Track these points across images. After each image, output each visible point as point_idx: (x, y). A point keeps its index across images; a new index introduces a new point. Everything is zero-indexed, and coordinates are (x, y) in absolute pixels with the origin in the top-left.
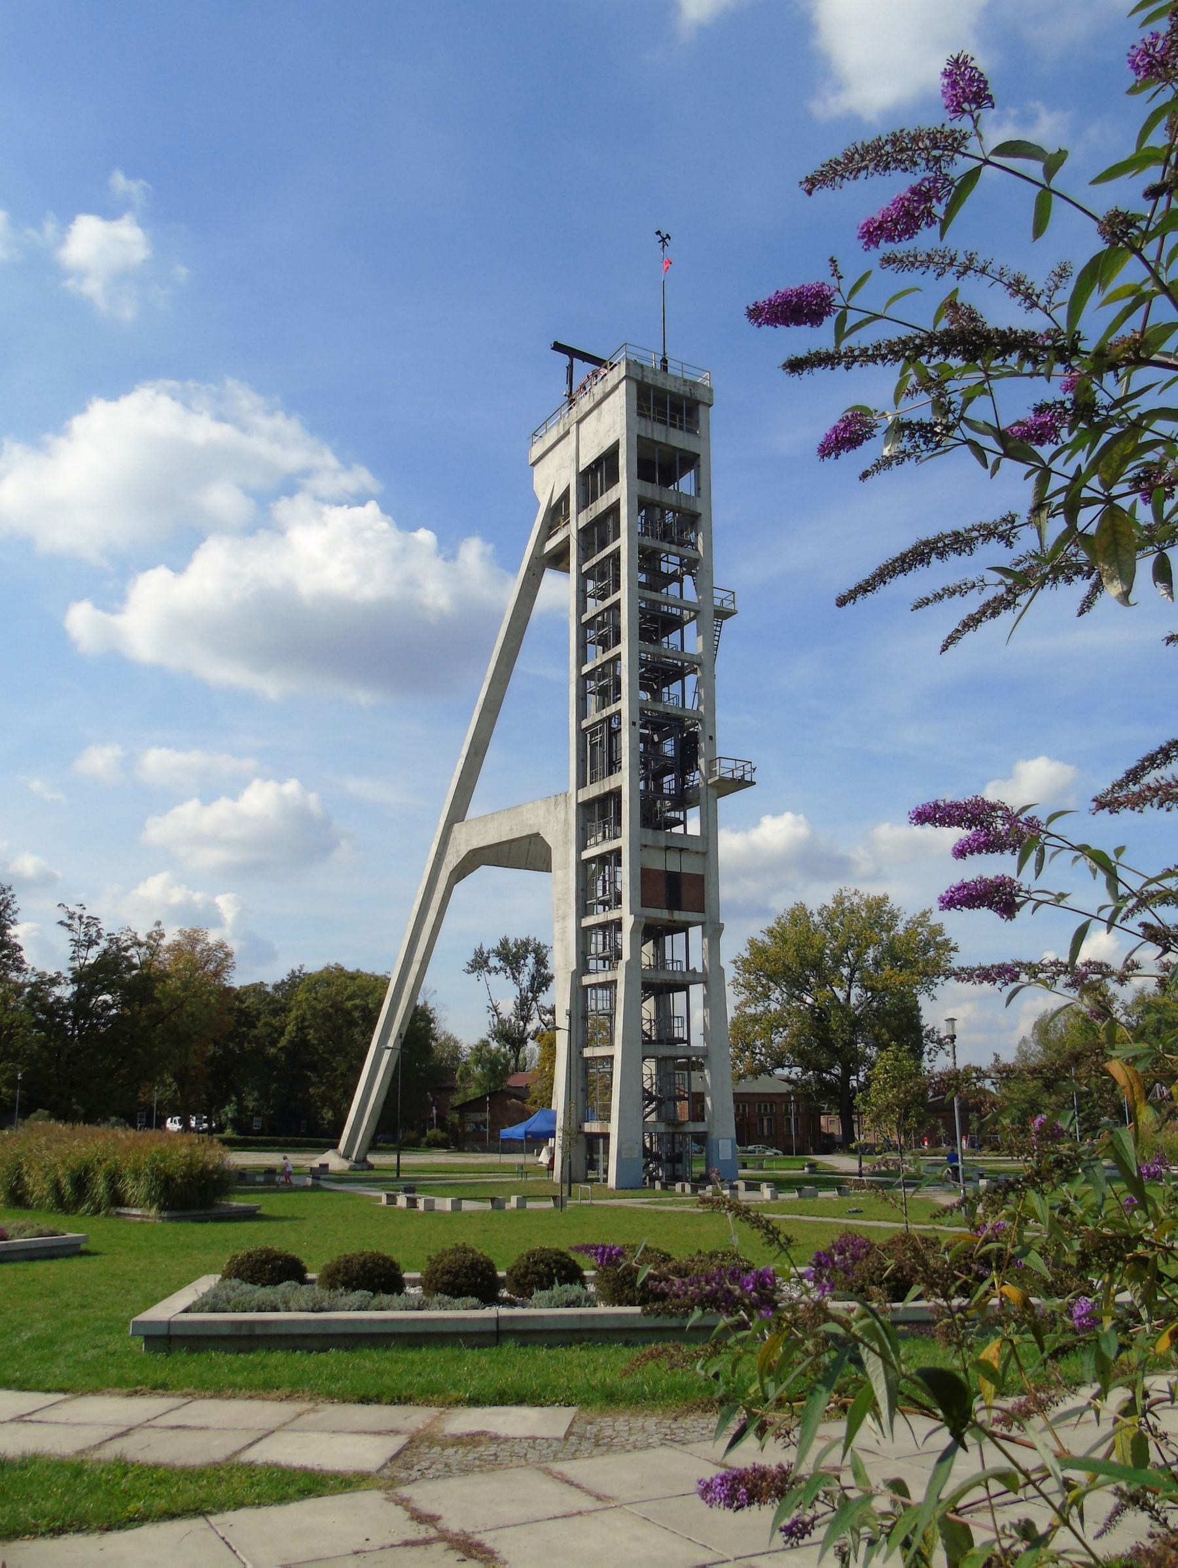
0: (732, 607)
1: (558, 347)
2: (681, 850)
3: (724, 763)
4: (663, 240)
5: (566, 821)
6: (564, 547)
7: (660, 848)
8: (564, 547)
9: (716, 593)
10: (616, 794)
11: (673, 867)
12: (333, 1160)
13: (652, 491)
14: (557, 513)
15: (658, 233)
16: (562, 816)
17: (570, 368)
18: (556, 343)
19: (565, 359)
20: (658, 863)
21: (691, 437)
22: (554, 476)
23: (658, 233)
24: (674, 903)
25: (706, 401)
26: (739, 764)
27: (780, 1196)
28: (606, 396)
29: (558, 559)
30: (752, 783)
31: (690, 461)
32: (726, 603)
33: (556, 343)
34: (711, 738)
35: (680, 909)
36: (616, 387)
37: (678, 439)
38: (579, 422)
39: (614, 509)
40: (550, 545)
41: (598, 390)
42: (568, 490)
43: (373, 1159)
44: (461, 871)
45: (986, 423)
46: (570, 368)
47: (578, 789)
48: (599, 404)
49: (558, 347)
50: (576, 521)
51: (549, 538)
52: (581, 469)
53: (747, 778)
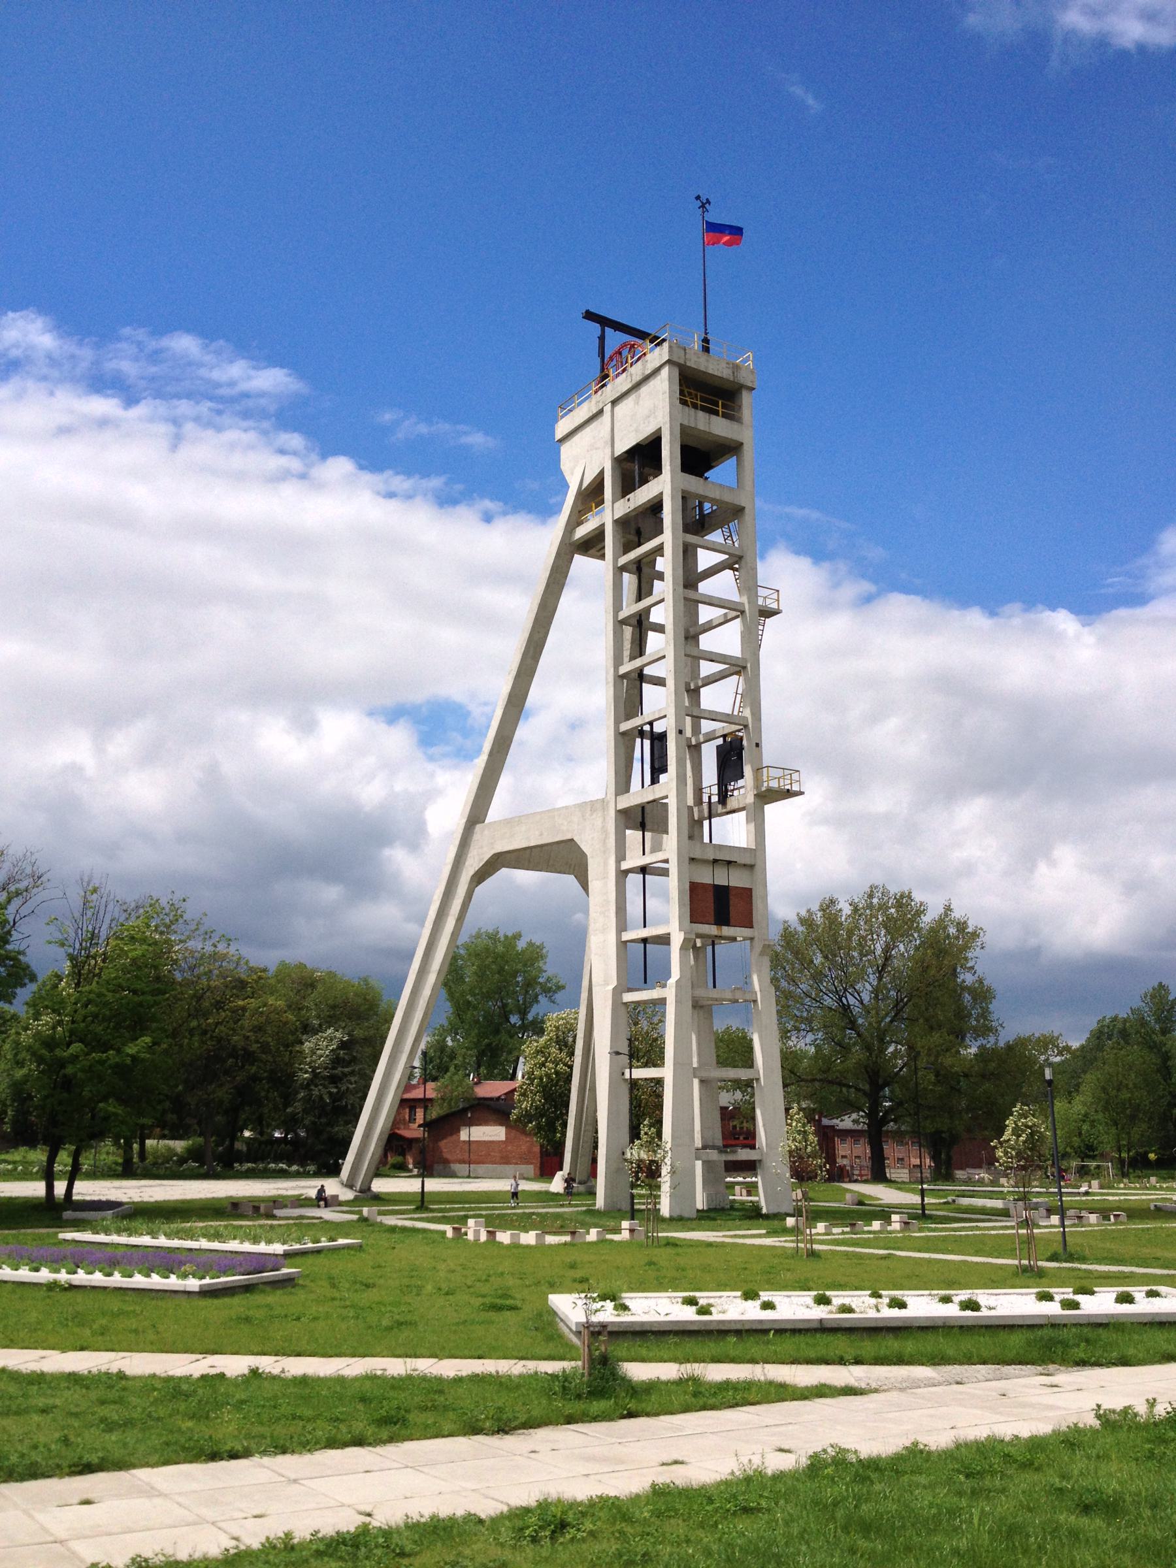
0: (774, 606)
1: (590, 316)
2: (729, 863)
3: (774, 773)
4: (703, 206)
5: (604, 830)
6: (599, 535)
7: (705, 862)
8: (599, 535)
9: (761, 592)
10: (663, 1001)
11: (721, 880)
12: (332, 1187)
13: (693, 483)
14: (592, 495)
15: (698, 198)
16: (599, 822)
17: (602, 339)
18: (588, 312)
19: (596, 328)
20: (706, 877)
21: (735, 425)
22: (586, 456)
23: (698, 198)
24: (722, 919)
25: (750, 385)
26: (787, 772)
27: (835, 1230)
28: (646, 379)
29: (592, 545)
30: (802, 793)
31: (731, 449)
32: (768, 601)
33: (588, 312)
34: (757, 745)
35: (728, 924)
36: (657, 371)
37: (719, 427)
38: (614, 402)
39: (655, 507)
40: (581, 532)
41: (637, 371)
42: (602, 472)
43: (380, 1186)
44: (481, 876)
45: (1092, 1293)
46: (602, 339)
47: (616, 795)
48: (637, 386)
49: (590, 316)
50: (610, 512)
51: (580, 523)
52: (617, 453)
53: (795, 788)
